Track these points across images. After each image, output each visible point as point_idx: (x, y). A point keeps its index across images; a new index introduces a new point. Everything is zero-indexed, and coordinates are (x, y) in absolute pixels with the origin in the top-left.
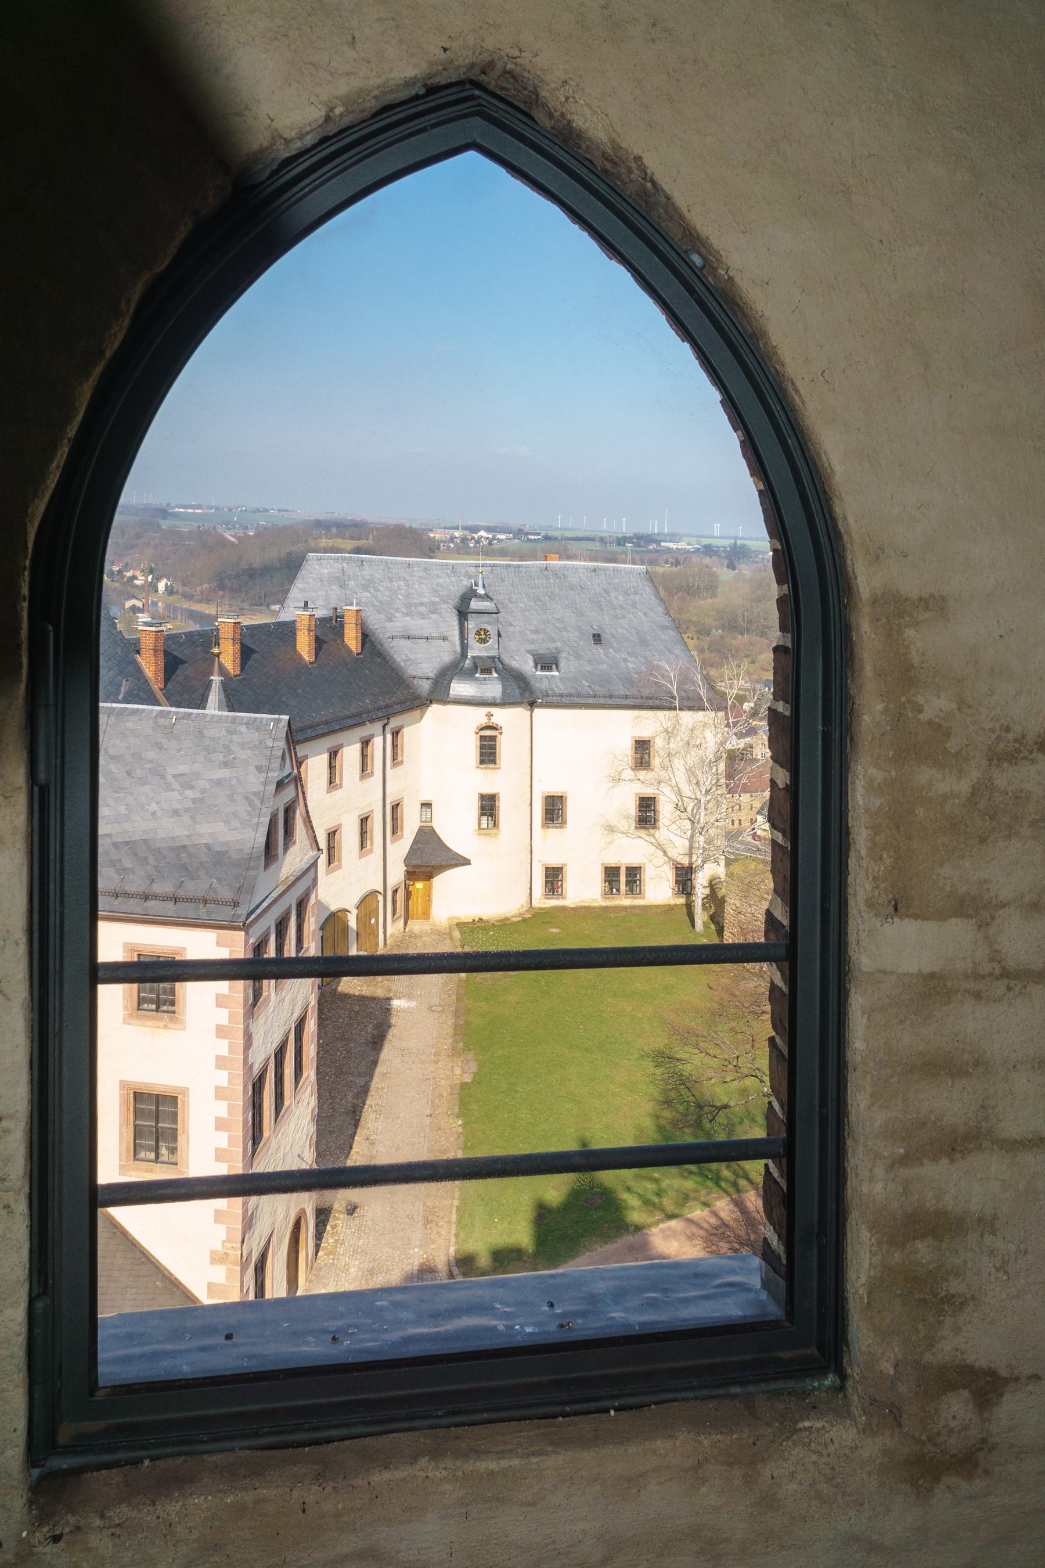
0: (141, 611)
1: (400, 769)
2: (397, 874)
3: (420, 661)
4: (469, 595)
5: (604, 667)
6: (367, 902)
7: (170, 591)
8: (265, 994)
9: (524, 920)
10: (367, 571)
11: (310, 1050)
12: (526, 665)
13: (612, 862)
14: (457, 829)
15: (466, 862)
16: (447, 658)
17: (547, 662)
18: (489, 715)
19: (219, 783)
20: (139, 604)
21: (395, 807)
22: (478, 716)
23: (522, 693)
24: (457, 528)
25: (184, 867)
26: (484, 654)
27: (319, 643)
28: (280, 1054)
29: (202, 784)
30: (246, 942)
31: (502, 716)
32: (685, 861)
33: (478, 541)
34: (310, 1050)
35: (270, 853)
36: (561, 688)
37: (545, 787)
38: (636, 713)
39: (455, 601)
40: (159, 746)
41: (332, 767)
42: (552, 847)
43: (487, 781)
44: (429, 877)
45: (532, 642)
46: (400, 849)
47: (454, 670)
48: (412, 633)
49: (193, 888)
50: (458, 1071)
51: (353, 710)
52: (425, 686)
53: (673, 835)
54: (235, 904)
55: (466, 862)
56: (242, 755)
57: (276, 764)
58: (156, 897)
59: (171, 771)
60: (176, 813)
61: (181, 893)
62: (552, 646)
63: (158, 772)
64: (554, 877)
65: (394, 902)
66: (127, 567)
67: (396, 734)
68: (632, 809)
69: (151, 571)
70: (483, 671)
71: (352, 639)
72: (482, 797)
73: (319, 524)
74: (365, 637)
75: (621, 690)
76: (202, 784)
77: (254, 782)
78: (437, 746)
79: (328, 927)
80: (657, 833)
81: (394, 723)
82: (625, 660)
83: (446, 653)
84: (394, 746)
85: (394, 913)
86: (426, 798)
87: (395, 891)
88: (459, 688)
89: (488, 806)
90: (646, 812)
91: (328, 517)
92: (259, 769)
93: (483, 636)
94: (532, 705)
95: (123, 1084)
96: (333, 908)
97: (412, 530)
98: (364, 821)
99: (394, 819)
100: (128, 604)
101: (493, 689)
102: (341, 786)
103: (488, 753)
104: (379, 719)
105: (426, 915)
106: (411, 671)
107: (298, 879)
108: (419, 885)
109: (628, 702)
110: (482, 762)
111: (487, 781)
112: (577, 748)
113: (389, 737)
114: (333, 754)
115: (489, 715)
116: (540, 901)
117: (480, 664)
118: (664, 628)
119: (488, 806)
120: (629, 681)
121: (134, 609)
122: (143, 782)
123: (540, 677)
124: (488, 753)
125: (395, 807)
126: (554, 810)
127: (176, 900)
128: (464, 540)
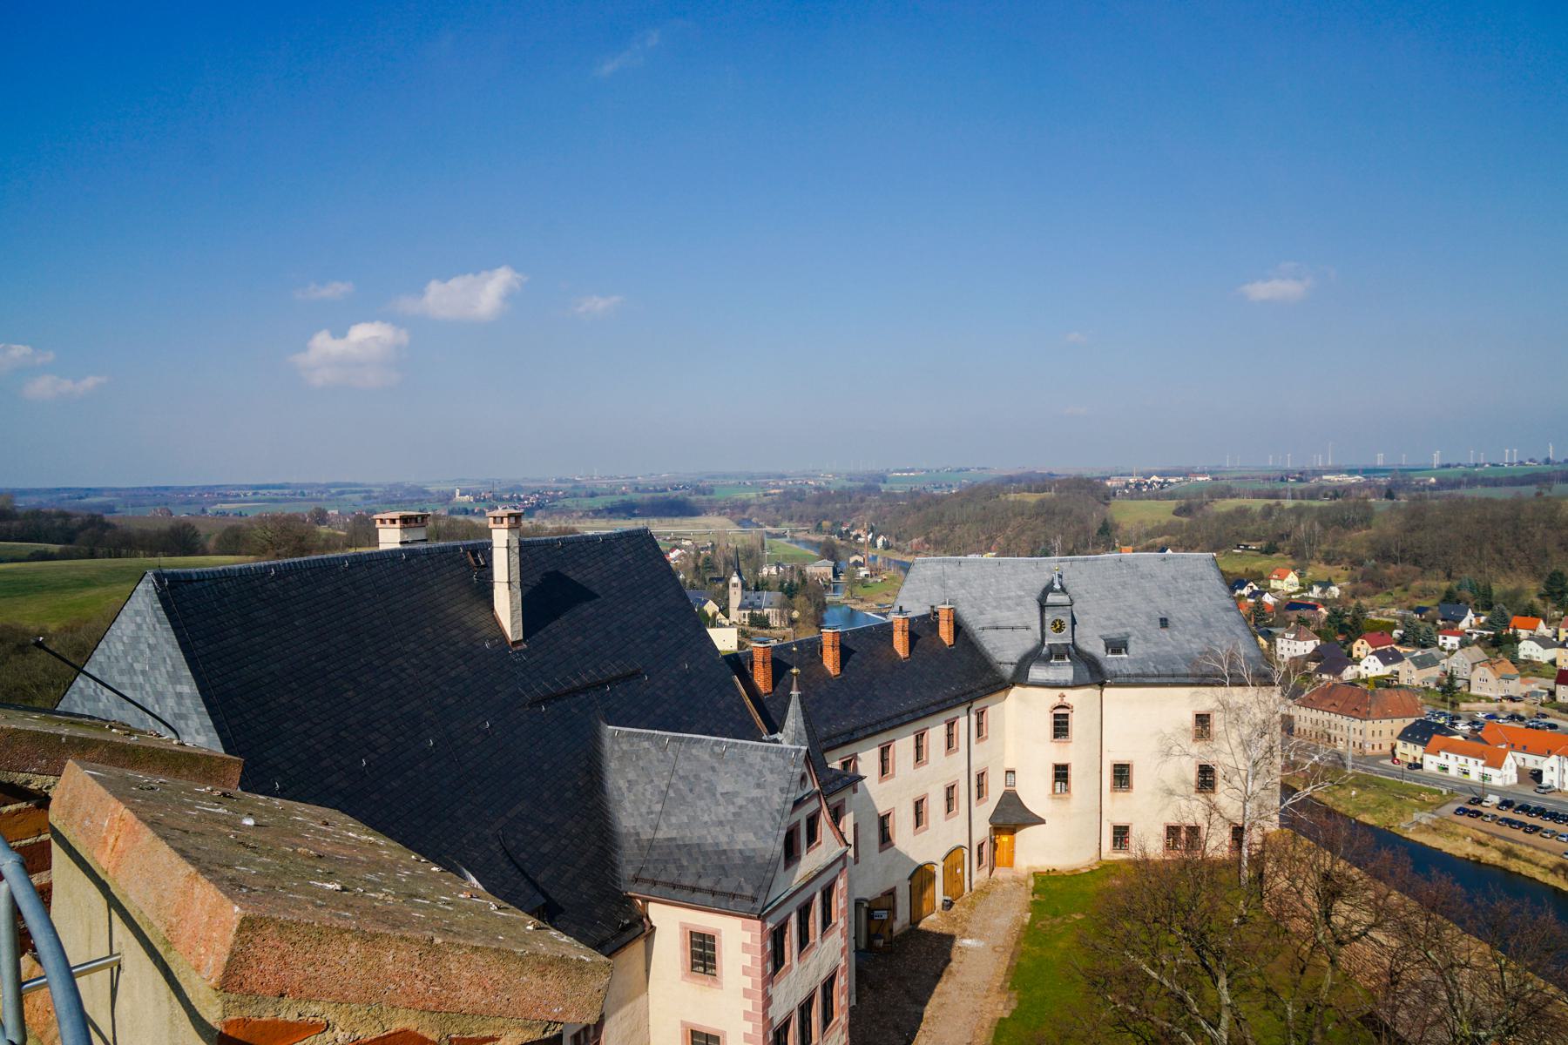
0: (862, 565)
1: (985, 744)
2: (982, 830)
3: (1005, 649)
4: (1049, 589)
5: (1169, 648)
6: (953, 855)
7: (887, 546)
8: (787, 963)
9: (1092, 871)
10: (964, 570)
11: (841, 1001)
12: (1096, 648)
13: (1173, 822)
14: (1035, 793)
15: (1042, 821)
16: (1029, 645)
17: (1117, 646)
18: (1062, 696)
19: (752, 800)
20: (861, 559)
21: (981, 776)
22: (1052, 697)
23: (1094, 675)
24: (1131, 475)
25: (723, 867)
26: (1059, 642)
27: (913, 638)
28: (805, 1008)
29: (740, 801)
30: (763, 929)
31: (1072, 696)
32: (1240, 823)
33: (1150, 486)
34: (841, 1001)
35: (791, 853)
36: (1132, 669)
37: (1113, 756)
38: (1194, 689)
39: (1037, 594)
40: (713, 769)
41: (918, 748)
42: (1119, 809)
43: (1059, 753)
44: (1012, 831)
45: (1104, 628)
46: (984, 813)
47: (1035, 656)
48: (1000, 624)
49: (727, 885)
50: (1001, 1007)
51: (939, 698)
52: (1009, 671)
53: (1227, 798)
54: (754, 900)
55: (1042, 821)
56: (770, 777)
57: (793, 788)
58: (700, 890)
59: (720, 790)
60: (721, 823)
61: (718, 888)
62: (1122, 630)
63: (711, 790)
64: (1121, 834)
65: (980, 854)
66: (853, 527)
67: (980, 714)
68: (1193, 775)
69: (872, 530)
70: (1057, 658)
71: (945, 633)
72: (1057, 767)
73: (1011, 479)
74: (959, 628)
75: (1184, 669)
76: (740, 801)
77: (777, 799)
78: (1017, 727)
79: (916, 877)
80: (1212, 796)
81: (977, 705)
82: (1189, 641)
83: (1028, 641)
84: (979, 724)
85: (980, 863)
86: (1009, 766)
87: (980, 847)
88: (1036, 673)
89: (1061, 773)
90: (1206, 778)
91: (1020, 471)
92: (782, 790)
93: (1058, 626)
94: (1102, 685)
95: (683, 1024)
96: (921, 862)
97: (1089, 481)
98: (950, 790)
99: (980, 786)
100: (852, 560)
101: (1066, 672)
102: (893, 776)
103: (1061, 727)
104: (962, 704)
105: (1011, 863)
106: (998, 657)
107: (820, 873)
108: (1005, 839)
109: (1189, 680)
110: (1056, 736)
111: (1059, 753)
112: (1141, 724)
113: (974, 717)
114: (919, 738)
115: (1062, 696)
116: (1109, 853)
117: (1055, 650)
118: (1228, 610)
119: (1061, 773)
120: (1191, 661)
121: (857, 564)
122: (701, 798)
123: (1111, 662)
124: (1061, 727)
125: (981, 776)
126: (1122, 775)
127: (714, 894)
128: (1138, 486)
